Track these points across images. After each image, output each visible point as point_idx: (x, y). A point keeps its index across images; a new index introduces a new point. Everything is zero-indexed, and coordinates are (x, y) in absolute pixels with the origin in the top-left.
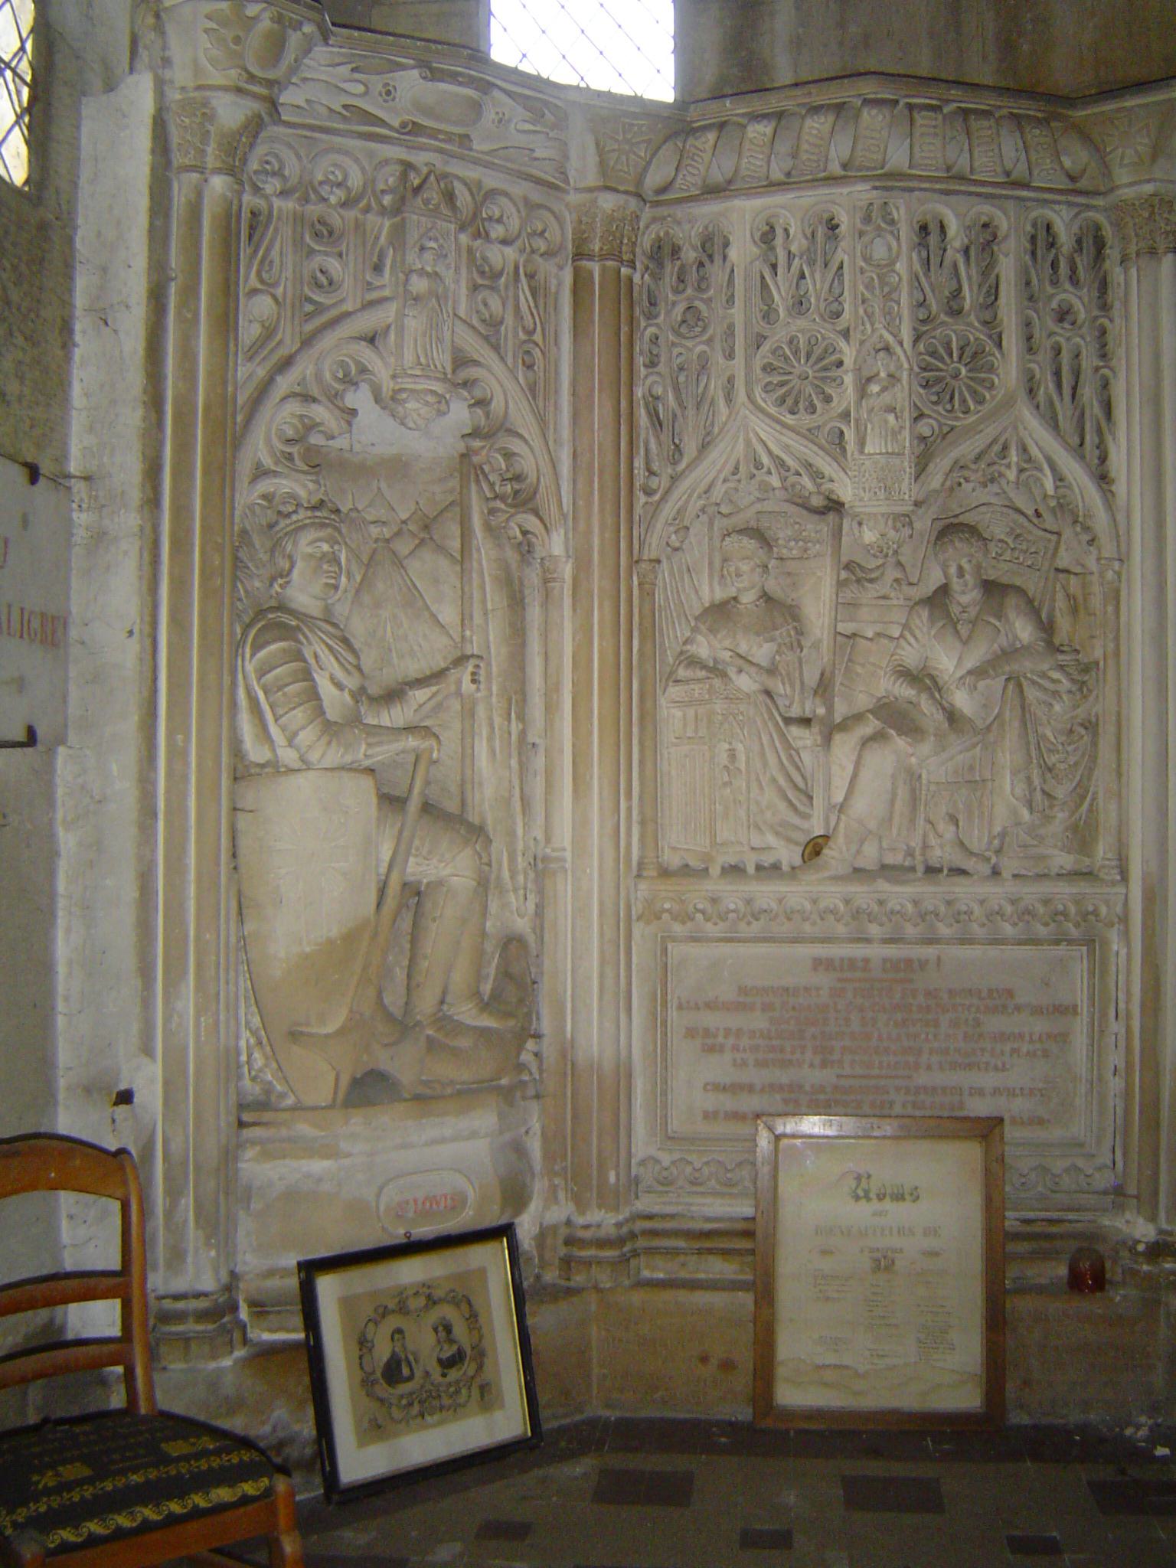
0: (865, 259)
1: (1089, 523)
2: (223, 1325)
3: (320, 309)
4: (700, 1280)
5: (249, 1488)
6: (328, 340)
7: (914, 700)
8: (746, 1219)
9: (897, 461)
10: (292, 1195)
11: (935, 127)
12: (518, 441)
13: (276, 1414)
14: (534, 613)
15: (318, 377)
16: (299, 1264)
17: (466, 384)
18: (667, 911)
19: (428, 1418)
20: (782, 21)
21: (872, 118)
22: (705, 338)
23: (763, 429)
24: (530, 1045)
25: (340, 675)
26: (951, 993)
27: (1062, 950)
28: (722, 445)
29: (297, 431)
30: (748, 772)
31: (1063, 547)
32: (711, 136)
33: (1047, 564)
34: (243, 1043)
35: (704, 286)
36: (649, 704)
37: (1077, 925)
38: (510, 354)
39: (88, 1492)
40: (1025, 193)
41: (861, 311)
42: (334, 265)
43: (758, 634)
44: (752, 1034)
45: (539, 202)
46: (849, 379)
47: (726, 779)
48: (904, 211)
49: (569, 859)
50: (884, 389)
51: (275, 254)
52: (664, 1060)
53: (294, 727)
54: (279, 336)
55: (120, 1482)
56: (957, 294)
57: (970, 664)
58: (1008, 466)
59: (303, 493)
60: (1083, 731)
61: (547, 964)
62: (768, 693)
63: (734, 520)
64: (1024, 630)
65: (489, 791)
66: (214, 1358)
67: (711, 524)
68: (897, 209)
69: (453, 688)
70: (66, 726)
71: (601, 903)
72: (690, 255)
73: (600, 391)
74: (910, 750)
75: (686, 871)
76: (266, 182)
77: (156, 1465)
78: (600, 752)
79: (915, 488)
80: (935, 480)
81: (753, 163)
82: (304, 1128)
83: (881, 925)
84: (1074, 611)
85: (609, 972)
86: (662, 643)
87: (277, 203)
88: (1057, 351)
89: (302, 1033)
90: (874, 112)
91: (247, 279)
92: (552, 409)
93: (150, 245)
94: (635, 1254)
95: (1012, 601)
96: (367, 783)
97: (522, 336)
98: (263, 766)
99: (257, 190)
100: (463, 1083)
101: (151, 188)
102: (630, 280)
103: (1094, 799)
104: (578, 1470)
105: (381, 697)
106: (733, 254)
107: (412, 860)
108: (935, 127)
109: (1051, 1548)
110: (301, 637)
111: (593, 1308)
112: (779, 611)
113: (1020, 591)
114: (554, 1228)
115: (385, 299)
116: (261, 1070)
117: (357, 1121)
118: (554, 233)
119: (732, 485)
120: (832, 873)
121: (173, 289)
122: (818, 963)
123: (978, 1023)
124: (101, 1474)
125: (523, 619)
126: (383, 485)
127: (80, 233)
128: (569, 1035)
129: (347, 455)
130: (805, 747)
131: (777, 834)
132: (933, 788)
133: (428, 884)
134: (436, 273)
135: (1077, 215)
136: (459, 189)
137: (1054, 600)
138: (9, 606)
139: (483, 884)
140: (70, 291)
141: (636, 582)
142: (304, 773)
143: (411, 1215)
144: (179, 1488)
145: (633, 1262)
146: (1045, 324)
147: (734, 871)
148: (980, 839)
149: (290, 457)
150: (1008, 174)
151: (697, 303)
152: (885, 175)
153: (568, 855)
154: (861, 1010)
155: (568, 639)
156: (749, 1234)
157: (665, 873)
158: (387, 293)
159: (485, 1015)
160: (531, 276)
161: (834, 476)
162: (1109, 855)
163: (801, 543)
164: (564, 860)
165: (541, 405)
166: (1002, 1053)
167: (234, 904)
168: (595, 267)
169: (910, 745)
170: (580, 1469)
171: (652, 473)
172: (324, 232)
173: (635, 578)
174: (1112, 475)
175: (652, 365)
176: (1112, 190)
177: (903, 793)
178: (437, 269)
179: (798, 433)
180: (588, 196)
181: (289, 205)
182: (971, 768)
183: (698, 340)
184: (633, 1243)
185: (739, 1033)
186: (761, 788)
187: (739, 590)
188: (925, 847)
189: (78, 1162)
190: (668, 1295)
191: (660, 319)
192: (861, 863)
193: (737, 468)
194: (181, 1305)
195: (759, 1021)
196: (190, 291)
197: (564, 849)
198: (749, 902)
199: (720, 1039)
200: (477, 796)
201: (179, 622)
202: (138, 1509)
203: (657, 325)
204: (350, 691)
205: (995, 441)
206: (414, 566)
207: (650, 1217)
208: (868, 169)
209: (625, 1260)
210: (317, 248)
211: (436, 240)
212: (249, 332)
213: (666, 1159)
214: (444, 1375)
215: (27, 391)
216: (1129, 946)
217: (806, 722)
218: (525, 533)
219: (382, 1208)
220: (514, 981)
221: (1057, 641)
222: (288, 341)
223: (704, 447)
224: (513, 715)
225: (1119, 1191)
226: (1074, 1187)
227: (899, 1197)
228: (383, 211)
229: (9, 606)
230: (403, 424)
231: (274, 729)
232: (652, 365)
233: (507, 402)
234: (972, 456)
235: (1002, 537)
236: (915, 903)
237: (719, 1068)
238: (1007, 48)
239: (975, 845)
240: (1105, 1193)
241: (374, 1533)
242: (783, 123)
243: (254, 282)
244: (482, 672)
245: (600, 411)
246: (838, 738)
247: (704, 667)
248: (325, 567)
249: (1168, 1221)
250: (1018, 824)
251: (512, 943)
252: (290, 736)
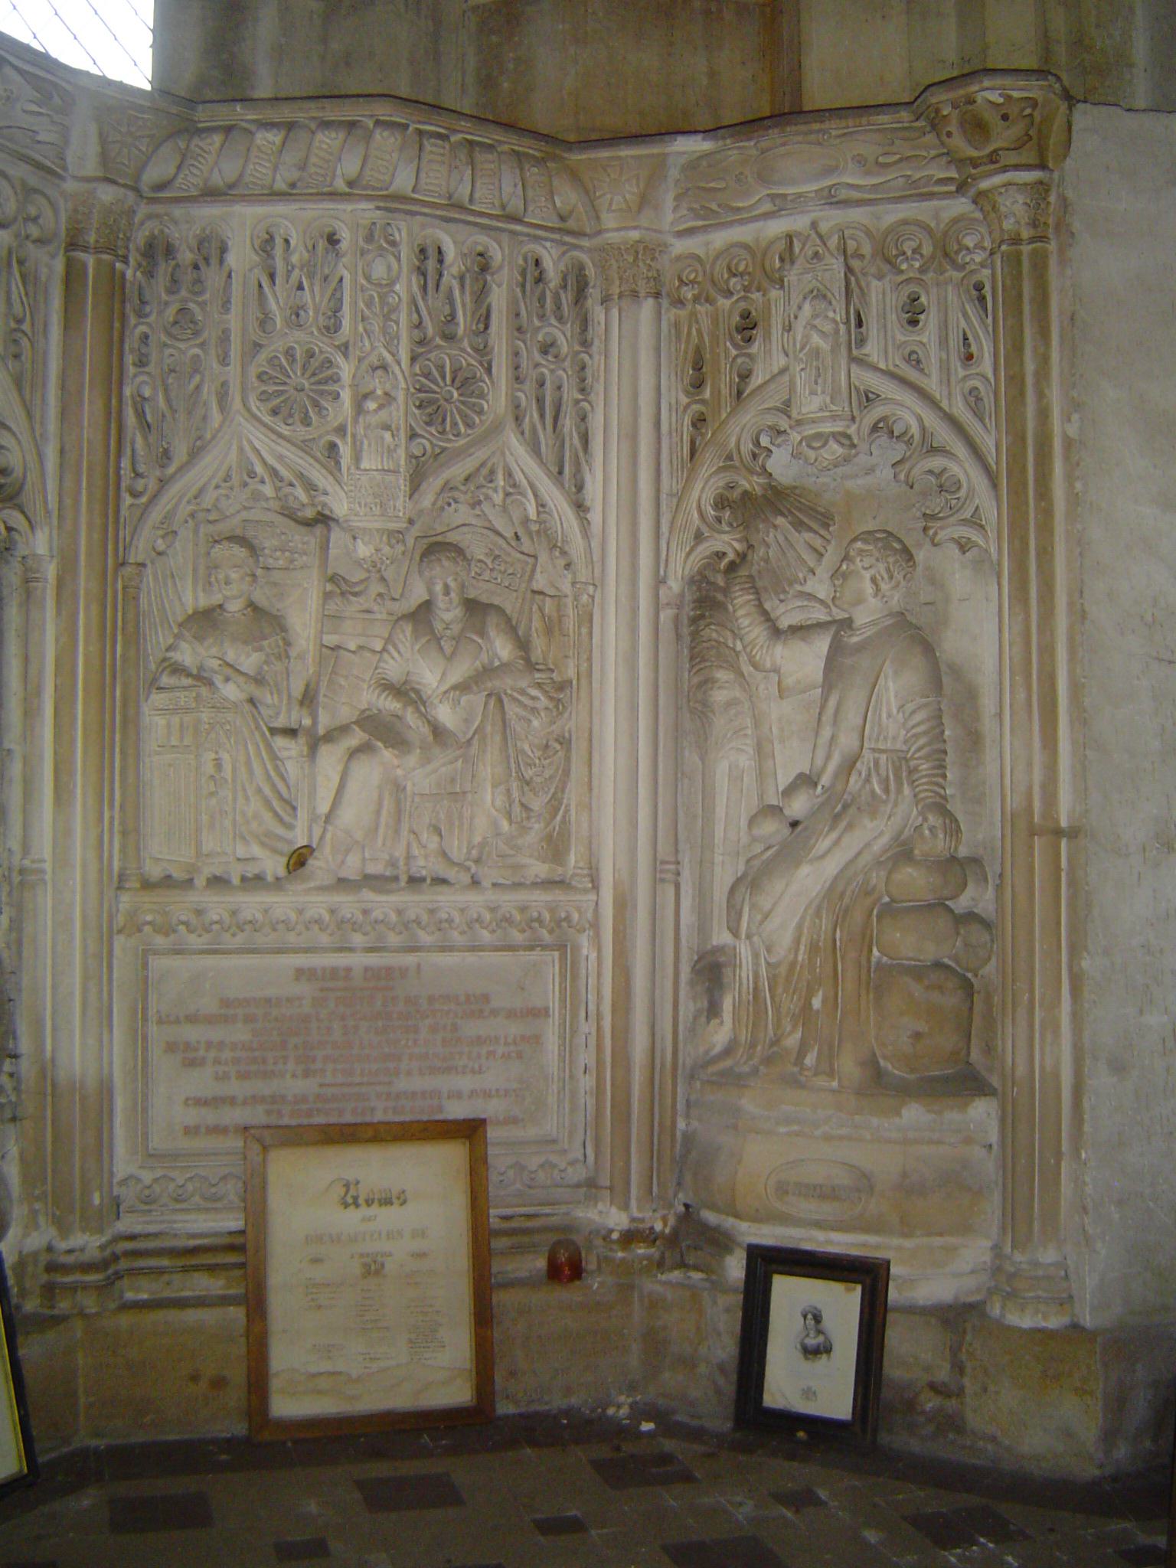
0: (368, 278)
1: (566, 548)
4: (187, 1298)
7: (400, 713)
9: (391, 478)
11: (443, 155)
18: (149, 923)
20: (265, 28)
21: (384, 139)
23: (259, 439)
24: (7, 1066)
26: (431, 999)
27: (535, 956)
30: (234, 780)
31: (539, 569)
32: (217, 139)
33: (524, 585)
37: (551, 932)
40: (519, 228)
41: (361, 329)
43: (246, 643)
44: (234, 1046)
46: (346, 396)
48: (405, 232)
50: (381, 407)
52: (145, 1075)
56: (452, 317)
57: (456, 676)
58: (495, 490)
60: (558, 747)
61: (25, 981)
62: (251, 701)
63: (220, 527)
64: (503, 649)
67: (196, 531)
68: (399, 230)
71: (84, 917)
72: (186, 256)
73: (91, 390)
74: (396, 762)
75: (167, 882)
79: (409, 505)
80: (427, 499)
81: (259, 171)
83: (365, 934)
84: (549, 631)
86: (146, 650)
88: (541, 384)
90: (386, 134)
92: (38, 402)
94: (118, 1276)
95: (492, 620)
97: (13, 325)
102: (123, 275)
103: (567, 811)
104: (86, 1502)
106: (231, 259)
108: (443, 155)
109: (575, 1526)
111: (79, 1334)
112: (264, 621)
113: (499, 610)
114: (35, 1255)
119: (223, 492)
120: (318, 883)
122: (300, 973)
123: (455, 1028)
128: (48, 1054)
130: (290, 758)
131: (263, 845)
132: (417, 799)
135: (564, 253)
137: (531, 620)
145: (118, 1284)
146: (530, 355)
147: (218, 882)
148: (459, 848)
150: (503, 207)
151: (191, 305)
152: (386, 196)
153: (48, 866)
154: (343, 1018)
156: (231, 1248)
157: (147, 885)
160: (21, 262)
161: (329, 489)
162: (581, 864)
163: (287, 554)
164: (43, 871)
165: (28, 397)
166: (479, 1056)
168: (90, 260)
169: (396, 757)
170: (87, 1500)
171: (138, 475)
174: (588, 503)
175: (141, 363)
176: (600, 232)
177: (388, 804)
179: (294, 444)
182: (453, 780)
183: (192, 342)
184: (115, 1265)
185: (221, 1045)
186: (247, 799)
187: (226, 598)
188: (409, 857)
191: (152, 319)
192: (344, 873)
195: (240, 1033)
198: (234, 913)
199: (202, 1052)
203: (149, 325)
205: (483, 464)
207: (132, 1237)
208: (374, 188)
209: (110, 1282)
213: (147, 1177)
216: (599, 951)
217: (291, 732)
221: (533, 659)
223: (195, 454)
225: (591, 1184)
226: (549, 1182)
227: (387, 1202)
232: (141, 363)
234: (463, 476)
235: (482, 557)
236: (399, 912)
237: (201, 1082)
238: (487, 83)
239: (456, 854)
240: (578, 1186)
242: (291, 134)
245: (91, 408)
246: (324, 750)
247: (189, 675)
249: (640, 1209)
250: (498, 835)
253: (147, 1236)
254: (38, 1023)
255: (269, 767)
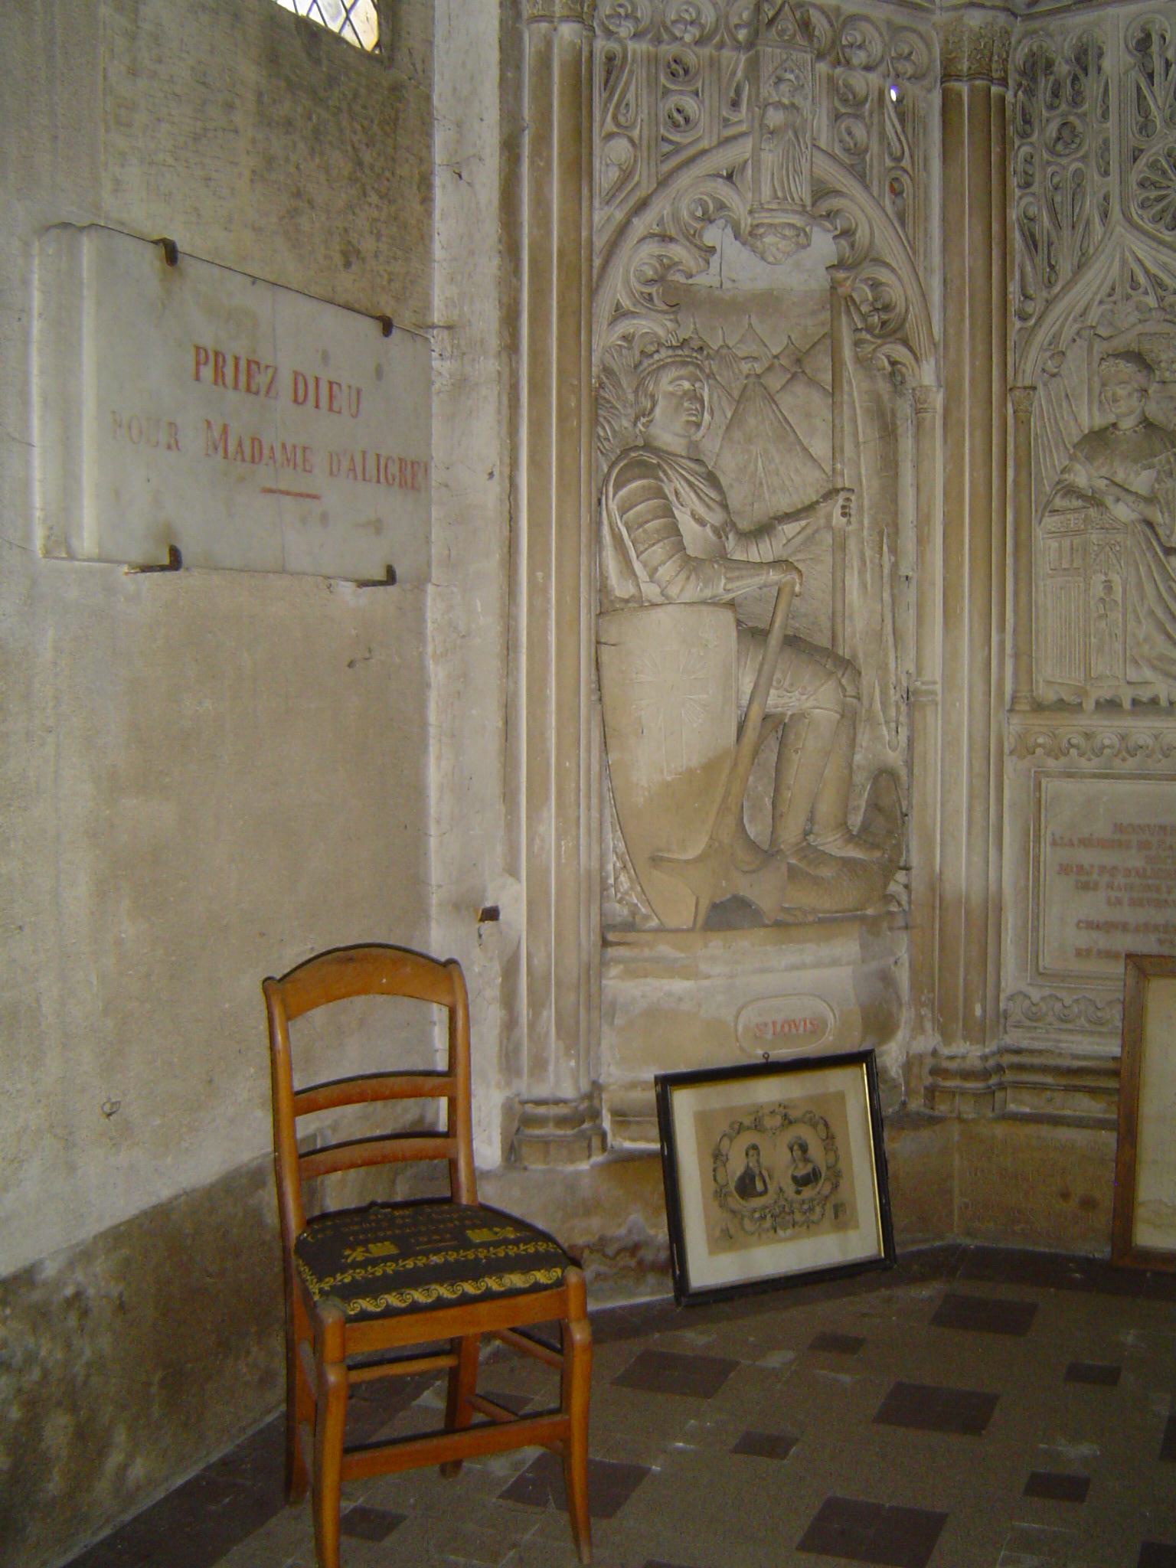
2: (582, 1133)
3: (678, 148)
4: (1064, 1117)
5: (541, 1277)
6: (684, 180)
8: (1114, 1058)
10: (654, 1013)
12: (884, 270)
13: (633, 1217)
14: (907, 445)
15: (675, 217)
16: (657, 1079)
17: (829, 216)
19: (781, 1233)
22: (1081, 153)
23: (1142, 249)
25: (701, 510)
28: (1097, 266)
29: (656, 271)
34: (610, 867)
35: (1078, 99)
36: (1023, 536)
38: (875, 183)
39: (390, 1268)
42: (690, 105)
43: (1136, 461)
44: (1128, 872)
45: (905, 23)
47: (1102, 611)
49: (939, 692)
51: (630, 96)
53: (655, 563)
54: (637, 178)
55: (421, 1261)
59: (661, 333)
61: (916, 799)
62: (1150, 524)
65: (860, 624)
66: (572, 1162)
69: (822, 522)
70: (429, 566)
72: (1063, 69)
73: (970, 216)
75: (1061, 706)
76: (619, 25)
77: (456, 1249)
78: (970, 585)
82: (665, 949)
85: (979, 809)
86: (1039, 473)
87: (631, 45)
89: (662, 859)
91: (602, 125)
92: (921, 236)
93: (501, 96)
94: (1002, 1087)
96: (727, 617)
97: (889, 163)
98: (627, 601)
99: (609, 34)
100: (825, 912)
101: (500, 41)
102: (1002, 99)
105: (750, 532)
106: (1106, 64)
107: (772, 691)
110: (661, 474)
114: (920, 1057)
115: (743, 134)
116: (626, 893)
117: (716, 944)
118: (921, 56)
121: (526, 139)
124: (404, 1255)
125: (896, 452)
126: (754, 321)
127: (437, 90)
129: (717, 293)
131: (1154, 668)
133: (792, 716)
134: (793, 105)
136: (816, 17)
138: (364, 453)
139: (850, 718)
140: (429, 147)
141: (1010, 411)
142: (664, 608)
143: (769, 1036)
144: (474, 1271)
147: (1111, 706)
149: (650, 298)
151: (1071, 118)
155: (933, 469)
156: (1115, 1073)
157: (1039, 707)
158: (744, 128)
159: (851, 846)
164: (933, 693)
167: (596, 735)
168: (964, 88)
170: (927, 1292)
171: (1027, 297)
172: (678, 70)
173: (1010, 405)
178: (796, 102)
180: (952, 14)
181: (642, 47)
189: (408, 969)
190: (1030, 1129)
191: (1035, 138)
193: (1113, 289)
194: (542, 1110)
195: (1135, 860)
196: (542, 140)
197: (935, 683)
198: (1123, 738)
199: (1095, 877)
200: (848, 630)
201: (537, 464)
202: (433, 1286)
203: (1031, 144)
204: (712, 526)
206: (786, 401)
207: (1018, 1052)
209: (991, 1092)
210: (672, 87)
211: (792, 71)
212: (605, 176)
213: (1035, 995)
214: (798, 1192)
215: (383, 247)
218: (893, 363)
219: (740, 1028)
220: (884, 815)
222: (644, 184)
223: (1080, 268)
224: (885, 548)
228: (738, 46)
229: (364, 453)
230: (763, 258)
231: (637, 566)
233: (871, 228)
237: (1093, 905)
241: (715, 1336)
243: (610, 126)
244: (853, 505)
248: (686, 404)
251: (884, 776)
252: (655, 572)
253: (1032, 1052)
254: (928, 840)
255: (1162, 588)
